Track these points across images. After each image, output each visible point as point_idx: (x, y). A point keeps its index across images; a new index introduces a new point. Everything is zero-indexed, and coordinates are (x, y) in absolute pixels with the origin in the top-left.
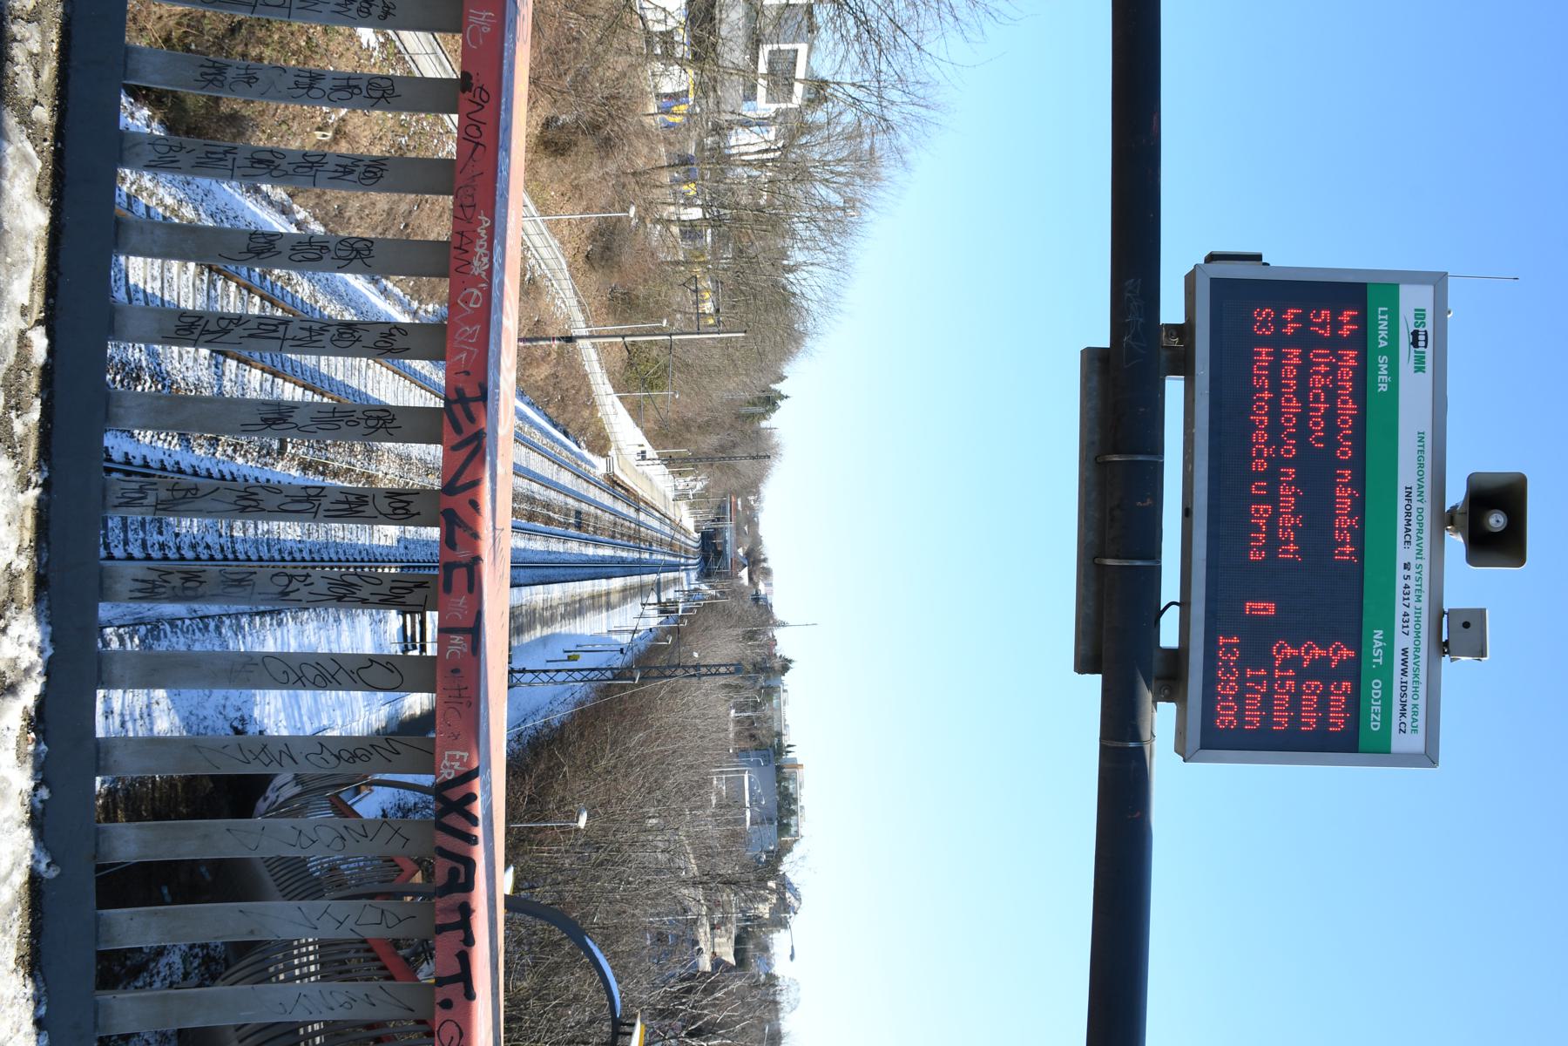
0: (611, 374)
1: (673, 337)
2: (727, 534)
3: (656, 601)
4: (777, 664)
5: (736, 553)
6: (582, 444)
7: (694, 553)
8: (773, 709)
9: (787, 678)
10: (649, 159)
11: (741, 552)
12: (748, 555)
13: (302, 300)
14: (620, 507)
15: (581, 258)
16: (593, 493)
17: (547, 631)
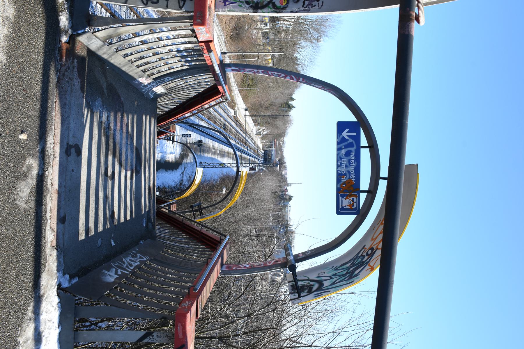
0: (237, 83)
1: (260, 54)
2: (273, 152)
3: (248, 163)
4: (288, 197)
5: (275, 160)
6: (227, 103)
7: (261, 157)
8: (286, 213)
9: (291, 203)
10: (241, 315)
11: (277, 159)
12: (279, 161)
13: (139, 12)
14: (238, 129)
15: (229, 37)
16: (229, 120)
17: (213, 156)
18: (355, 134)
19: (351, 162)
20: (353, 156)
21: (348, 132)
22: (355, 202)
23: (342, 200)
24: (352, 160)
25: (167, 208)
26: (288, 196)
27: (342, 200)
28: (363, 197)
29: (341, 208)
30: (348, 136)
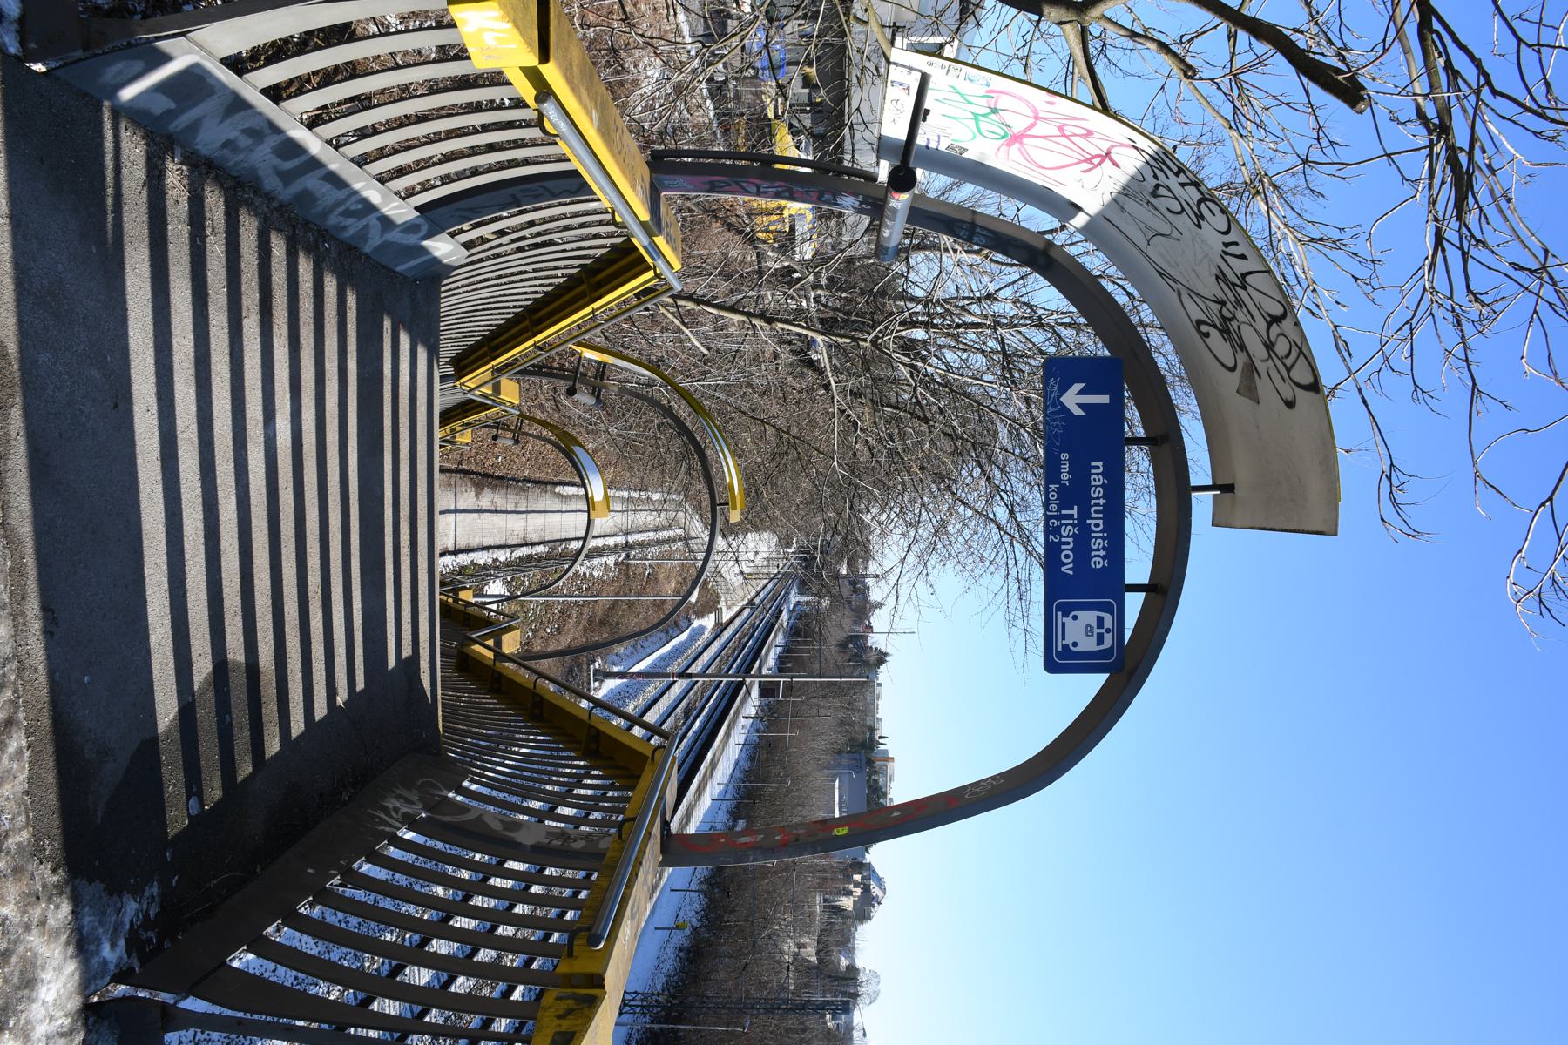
4: (873, 658)
18: (1104, 399)
19: (1095, 547)
20: (1097, 474)
22: (1108, 631)
23: (1063, 624)
24: (1096, 486)
25: (490, 643)
26: (874, 653)
27: (1063, 624)
28: (1134, 604)
29: (1060, 649)
30: (1080, 405)
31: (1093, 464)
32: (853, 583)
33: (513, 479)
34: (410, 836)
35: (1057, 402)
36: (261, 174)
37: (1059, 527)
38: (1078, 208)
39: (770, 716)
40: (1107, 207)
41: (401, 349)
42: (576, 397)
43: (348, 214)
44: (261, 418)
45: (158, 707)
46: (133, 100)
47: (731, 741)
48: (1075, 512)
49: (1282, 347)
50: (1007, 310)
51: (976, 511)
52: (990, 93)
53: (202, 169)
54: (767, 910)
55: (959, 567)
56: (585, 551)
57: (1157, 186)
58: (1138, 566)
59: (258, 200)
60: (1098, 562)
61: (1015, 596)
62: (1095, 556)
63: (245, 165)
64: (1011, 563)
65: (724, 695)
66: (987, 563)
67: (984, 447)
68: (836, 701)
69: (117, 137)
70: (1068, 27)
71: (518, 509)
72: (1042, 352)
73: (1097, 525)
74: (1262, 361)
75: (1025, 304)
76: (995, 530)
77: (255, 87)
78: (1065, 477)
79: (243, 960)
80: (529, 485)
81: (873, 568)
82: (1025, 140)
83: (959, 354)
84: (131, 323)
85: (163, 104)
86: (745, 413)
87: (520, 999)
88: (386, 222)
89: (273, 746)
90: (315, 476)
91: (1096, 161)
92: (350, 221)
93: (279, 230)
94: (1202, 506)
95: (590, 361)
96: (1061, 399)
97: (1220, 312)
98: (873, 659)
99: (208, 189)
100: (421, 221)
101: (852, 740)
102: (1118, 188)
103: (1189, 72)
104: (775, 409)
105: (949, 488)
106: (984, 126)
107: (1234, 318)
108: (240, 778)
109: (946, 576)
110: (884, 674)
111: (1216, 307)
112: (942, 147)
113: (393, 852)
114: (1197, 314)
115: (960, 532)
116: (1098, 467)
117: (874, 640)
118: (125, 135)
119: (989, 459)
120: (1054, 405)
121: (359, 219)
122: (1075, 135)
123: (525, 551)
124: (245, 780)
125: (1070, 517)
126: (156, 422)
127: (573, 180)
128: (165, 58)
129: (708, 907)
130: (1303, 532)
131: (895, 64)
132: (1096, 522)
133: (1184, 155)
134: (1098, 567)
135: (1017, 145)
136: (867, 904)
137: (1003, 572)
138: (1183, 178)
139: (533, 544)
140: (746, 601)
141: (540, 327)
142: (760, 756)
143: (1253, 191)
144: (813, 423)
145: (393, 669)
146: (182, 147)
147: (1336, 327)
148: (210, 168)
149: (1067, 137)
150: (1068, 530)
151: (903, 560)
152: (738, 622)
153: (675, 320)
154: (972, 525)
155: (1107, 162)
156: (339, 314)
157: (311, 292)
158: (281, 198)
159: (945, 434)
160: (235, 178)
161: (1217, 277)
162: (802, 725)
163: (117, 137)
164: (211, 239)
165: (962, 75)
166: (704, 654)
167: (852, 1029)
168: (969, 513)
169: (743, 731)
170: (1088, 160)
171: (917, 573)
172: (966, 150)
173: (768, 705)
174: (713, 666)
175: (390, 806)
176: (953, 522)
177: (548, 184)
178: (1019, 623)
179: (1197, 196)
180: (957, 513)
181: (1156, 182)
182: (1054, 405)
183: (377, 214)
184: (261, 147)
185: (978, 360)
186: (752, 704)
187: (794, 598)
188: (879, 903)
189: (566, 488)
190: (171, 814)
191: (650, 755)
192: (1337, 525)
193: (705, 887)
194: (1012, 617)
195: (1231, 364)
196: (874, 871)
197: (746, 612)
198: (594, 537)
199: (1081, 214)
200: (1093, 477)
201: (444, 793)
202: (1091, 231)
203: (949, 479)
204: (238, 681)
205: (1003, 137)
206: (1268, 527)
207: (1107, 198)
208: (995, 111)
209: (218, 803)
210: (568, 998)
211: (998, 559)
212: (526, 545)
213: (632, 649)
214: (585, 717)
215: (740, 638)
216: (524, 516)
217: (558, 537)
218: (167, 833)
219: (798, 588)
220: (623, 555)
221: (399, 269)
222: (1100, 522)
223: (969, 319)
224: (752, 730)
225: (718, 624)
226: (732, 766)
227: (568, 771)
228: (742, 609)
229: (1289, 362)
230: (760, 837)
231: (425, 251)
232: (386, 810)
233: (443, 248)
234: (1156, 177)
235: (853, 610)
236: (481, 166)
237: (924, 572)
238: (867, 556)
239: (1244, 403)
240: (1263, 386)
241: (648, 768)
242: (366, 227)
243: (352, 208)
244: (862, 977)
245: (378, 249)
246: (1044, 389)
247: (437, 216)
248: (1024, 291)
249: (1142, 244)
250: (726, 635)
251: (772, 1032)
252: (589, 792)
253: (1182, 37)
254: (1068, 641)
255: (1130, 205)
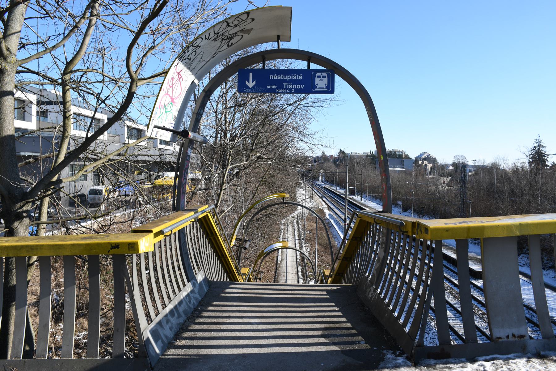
4: (342, 155)
18: (251, 75)
19: (296, 78)
21: (249, 82)
22: (321, 74)
23: (319, 88)
24: (277, 77)
27: (319, 88)
28: (313, 66)
29: (327, 89)
30: (253, 82)
31: (270, 78)
32: (315, 161)
33: (275, 277)
34: (379, 290)
35: (251, 89)
36: (179, 322)
37: (290, 89)
38: (193, 82)
39: (361, 192)
40: (193, 73)
41: (231, 291)
42: (247, 247)
43: (190, 301)
44: (250, 325)
45: (332, 350)
46: (159, 350)
47: (369, 205)
48: (285, 84)
49: (236, 22)
50: (221, 105)
51: (290, 117)
52: (160, 108)
53: (177, 336)
54: (430, 194)
55: (308, 123)
56: (300, 250)
57: (188, 59)
58: (302, 65)
59: (186, 324)
60: (300, 77)
61: (319, 104)
62: (299, 78)
63: (176, 326)
64: (307, 105)
65: (353, 208)
66: (308, 113)
67: (267, 115)
68: (357, 168)
69: (169, 355)
70: (138, 84)
71: (285, 276)
72: (235, 93)
73: (289, 77)
74: (240, 28)
75: (218, 99)
76: (296, 111)
77: (155, 318)
78: (274, 87)
79: (407, 329)
80: (277, 272)
81: (309, 154)
82: (173, 98)
83: (235, 122)
84: (222, 353)
85: (160, 342)
86: (254, 196)
87: (457, 280)
88: (192, 292)
89: (349, 325)
90: (268, 313)
91: (180, 77)
92: (192, 301)
93: (195, 320)
94: (284, 45)
95: (235, 243)
96: (251, 88)
97: (225, 40)
98: (342, 155)
99: (183, 336)
100: (192, 282)
101: (371, 163)
102: (188, 70)
103: (152, 48)
104: (252, 185)
105: (281, 126)
106: (168, 110)
107: (227, 36)
108: (357, 333)
109: (312, 128)
110: (348, 151)
111: (224, 41)
112: (174, 123)
113: (383, 295)
114: (226, 46)
115: (296, 122)
116: (272, 77)
117: (335, 155)
118: (169, 353)
119: (271, 112)
120: (252, 90)
121: (191, 299)
122: (172, 83)
123: (300, 274)
124: (357, 331)
125: (286, 85)
126: (250, 349)
127: (181, 232)
128: (148, 339)
129: (428, 215)
130: (291, 16)
131: (151, 135)
132: (288, 78)
133: (178, 50)
134: (302, 77)
135: (174, 100)
136: (429, 159)
137: (310, 108)
138: (186, 52)
139: (298, 271)
140: (321, 199)
141: (224, 255)
142: (375, 195)
143: (188, 27)
144: (258, 173)
145: (329, 296)
146: (171, 340)
147: (230, 2)
148: (177, 335)
149: (173, 85)
150: (291, 86)
151: (306, 142)
152: (328, 202)
153: (222, 215)
154: (294, 118)
155: (180, 73)
156: (220, 306)
157: (213, 313)
158: (185, 319)
159: (262, 127)
160: (180, 329)
161: (215, 41)
162: (365, 181)
163: (169, 355)
164: (198, 335)
165: (155, 116)
166: (338, 214)
167: (475, 165)
168: (290, 119)
169: (366, 201)
170: (180, 79)
171: (311, 138)
172: (175, 116)
173: (357, 192)
174: (343, 211)
175: (371, 296)
176: (293, 125)
177: (182, 243)
178: (328, 103)
179: (192, 47)
180: (289, 124)
181: (187, 59)
182: (252, 90)
183: (190, 294)
184: (171, 321)
185: (238, 115)
186: (357, 198)
187: (320, 182)
188: (430, 155)
189: (278, 259)
190: (364, 347)
191: (360, 218)
192: (289, 7)
193: (421, 216)
194: (326, 105)
195: (241, 36)
196: (418, 156)
197: (324, 199)
198: (296, 247)
199: (194, 81)
200: (274, 79)
201: (368, 281)
202: (200, 78)
203: (278, 126)
204: (327, 332)
205: (172, 104)
206: (290, 23)
207: (190, 73)
208: (165, 106)
209: (363, 337)
210: (417, 231)
211: (306, 109)
212: (298, 273)
213: (336, 239)
214: (349, 241)
215: (333, 201)
216: (288, 274)
217: (296, 263)
218: (369, 349)
219: (317, 181)
220: (302, 241)
221: (206, 291)
222: (288, 76)
223: (223, 118)
224: (366, 198)
225: (328, 209)
226: (378, 205)
227: (373, 257)
228: (323, 201)
229: (240, 20)
230: (384, 183)
231: (201, 283)
232: (372, 297)
233: (200, 277)
234: (185, 59)
235: (325, 162)
236: (169, 280)
237: (310, 135)
238: (307, 157)
239: (252, 33)
240: (248, 27)
241: (363, 219)
242: (194, 297)
243: (188, 300)
244: (456, 161)
245: (200, 296)
246: (247, 93)
247: (191, 278)
248: (214, 100)
249: (204, 63)
250: (332, 206)
251: (473, 193)
252: (393, 262)
253: (137, 48)
254: (325, 87)
255: (193, 66)
